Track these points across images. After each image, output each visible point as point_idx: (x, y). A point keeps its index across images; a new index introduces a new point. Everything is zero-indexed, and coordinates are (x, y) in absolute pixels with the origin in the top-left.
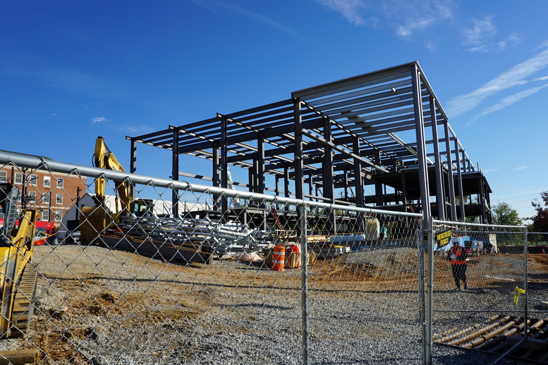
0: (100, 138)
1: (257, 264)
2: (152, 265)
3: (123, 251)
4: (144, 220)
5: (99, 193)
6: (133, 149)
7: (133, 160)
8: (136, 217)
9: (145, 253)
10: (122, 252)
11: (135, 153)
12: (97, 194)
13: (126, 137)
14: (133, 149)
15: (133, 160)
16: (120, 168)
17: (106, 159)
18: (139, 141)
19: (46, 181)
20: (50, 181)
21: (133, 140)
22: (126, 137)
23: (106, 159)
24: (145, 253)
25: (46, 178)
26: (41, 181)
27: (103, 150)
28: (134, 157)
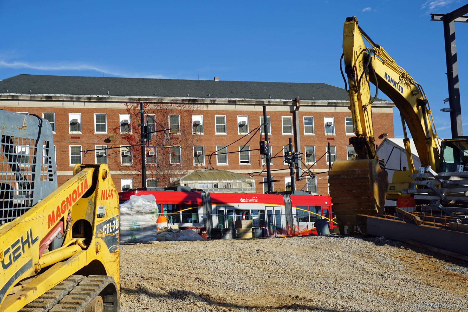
0: (350, 19)
1: (311, 234)
2: (444, 280)
3: (399, 247)
4: (454, 179)
5: (361, 132)
6: (449, 38)
7: (451, 60)
8: (435, 174)
9: (443, 251)
10: (394, 250)
11: (453, 45)
12: (357, 133)
13: (433, 15)
14: (449, 38)
15: (451, 60)
16: (403, 76)
17: (367, 60)
18: (459, 19)
19: (328, 125)
20: (333, 124)
21: (447, 19)
22: (433, 15)
23: (367, 60)
24: (443, 251)
25: (327, 120)
26: (320, 126)
27: (359, 43)
28: (453, 53)
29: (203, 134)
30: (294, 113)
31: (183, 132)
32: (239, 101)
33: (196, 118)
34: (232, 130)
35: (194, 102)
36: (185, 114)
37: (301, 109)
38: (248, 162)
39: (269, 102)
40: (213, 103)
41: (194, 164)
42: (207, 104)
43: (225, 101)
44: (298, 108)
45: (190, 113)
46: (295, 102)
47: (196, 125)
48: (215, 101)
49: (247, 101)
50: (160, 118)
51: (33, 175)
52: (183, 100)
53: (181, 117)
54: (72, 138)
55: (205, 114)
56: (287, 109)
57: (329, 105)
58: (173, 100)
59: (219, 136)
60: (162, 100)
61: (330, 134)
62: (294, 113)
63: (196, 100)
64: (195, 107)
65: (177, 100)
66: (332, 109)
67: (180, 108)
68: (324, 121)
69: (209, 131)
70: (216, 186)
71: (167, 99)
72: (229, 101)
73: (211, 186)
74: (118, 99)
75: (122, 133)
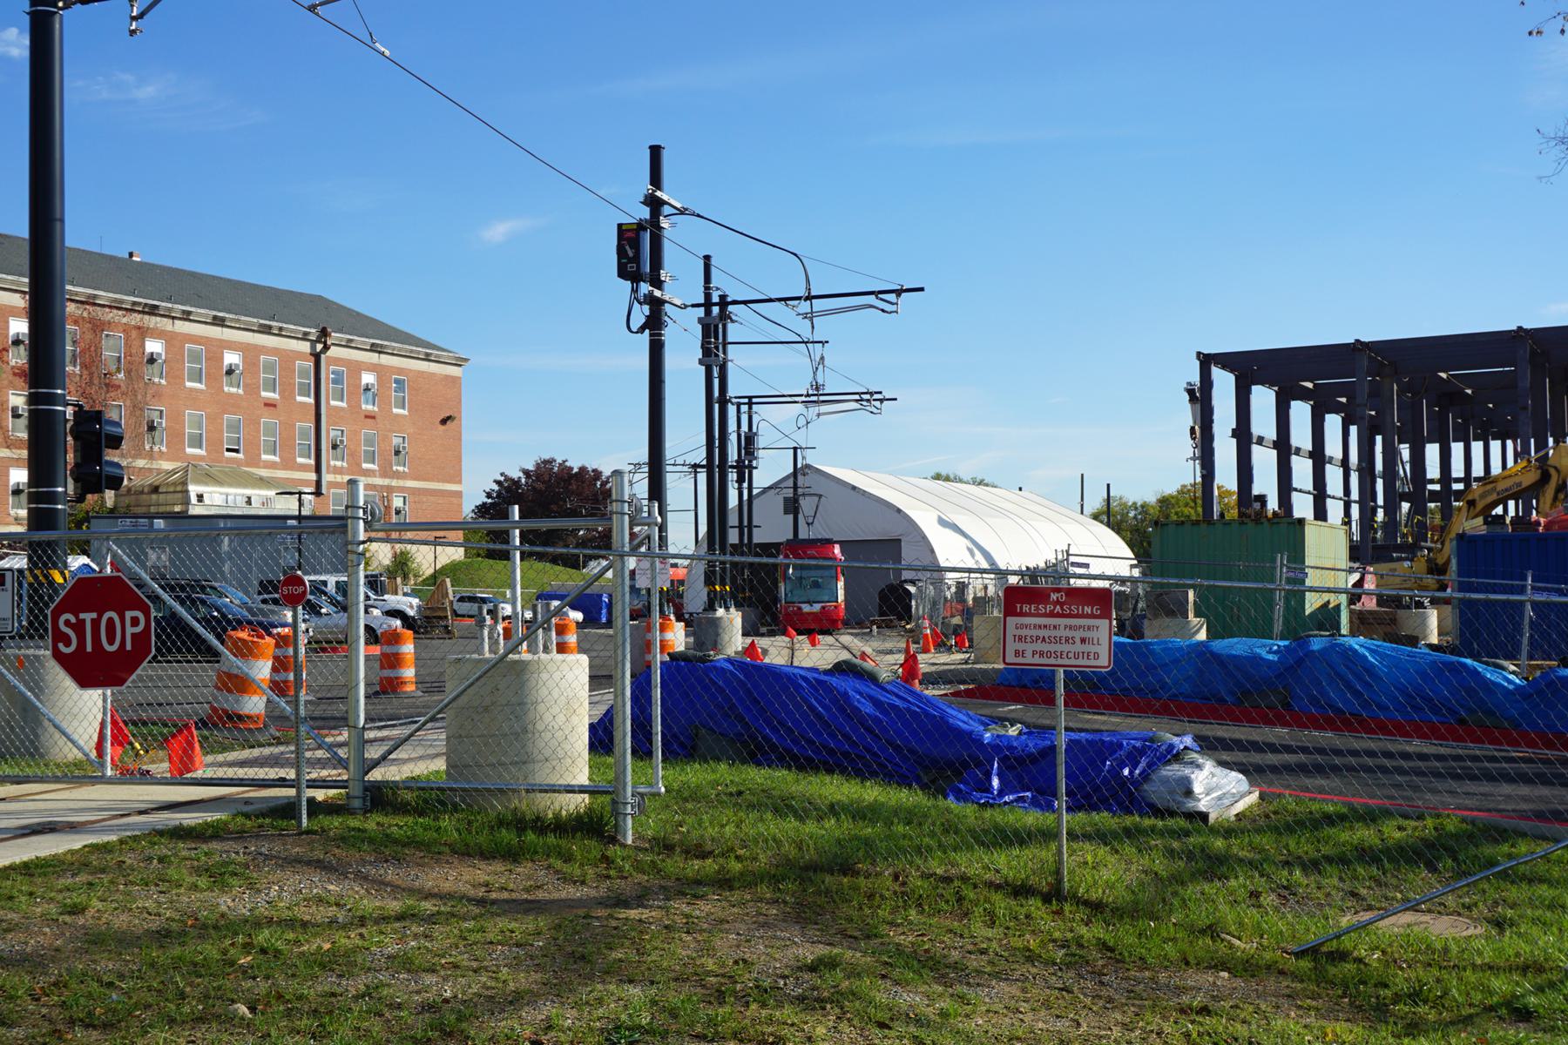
29: (163, 382)
30: (317, 357)
31: (128, 372)
32: (232, 320)
33: (153, 346)
34: (212, 380)
35: (153, 311)
36: (134, 334)
37: (334, 352)
38: (236, 451)
39: (281, 329)
40: (186, 316)
41: (147, 447)
42: (174, 318)
43: (206, 316)
44: (326, 348)
45: (144, 333)
46: (324, 333)
47: (152, 360)
48: (189, 313)
49: (245, 323)
50: (89, 336)
51: (318, 483)
52: (134, 303)
53: (126, 340)
54: (266, 405)
55: (169, 338)
56: (305, 347)
57: (374, 348)
58: (116, 300)
59: (191, 390)
60: (95, 296)
61: (370, 407)
62: (317, 357)
63: (156, 307)
64: (152, 321)
65: (122, 302)
66: (373, 358)
67: (124, 320)
68: (7, 328)
69: (176, 378)
70: (249, 502)
71: (104, 296)
72: (215, 318)
73: (241, 501)
74: (12, 282)
75: (13, 363)
